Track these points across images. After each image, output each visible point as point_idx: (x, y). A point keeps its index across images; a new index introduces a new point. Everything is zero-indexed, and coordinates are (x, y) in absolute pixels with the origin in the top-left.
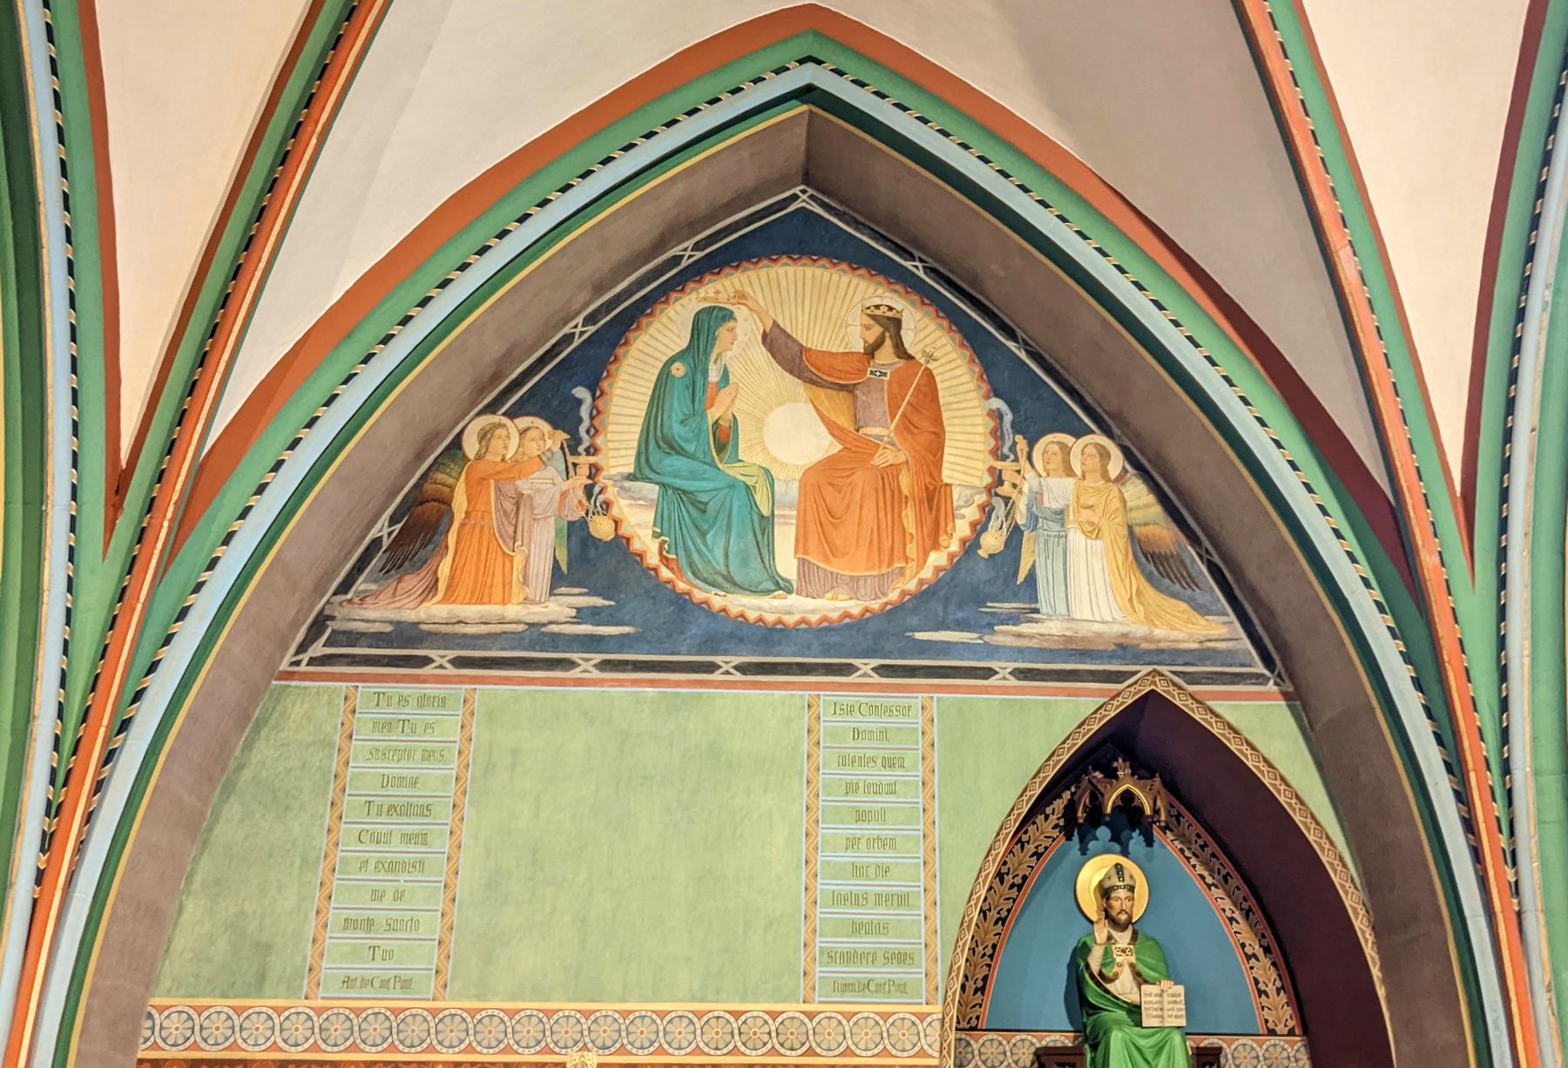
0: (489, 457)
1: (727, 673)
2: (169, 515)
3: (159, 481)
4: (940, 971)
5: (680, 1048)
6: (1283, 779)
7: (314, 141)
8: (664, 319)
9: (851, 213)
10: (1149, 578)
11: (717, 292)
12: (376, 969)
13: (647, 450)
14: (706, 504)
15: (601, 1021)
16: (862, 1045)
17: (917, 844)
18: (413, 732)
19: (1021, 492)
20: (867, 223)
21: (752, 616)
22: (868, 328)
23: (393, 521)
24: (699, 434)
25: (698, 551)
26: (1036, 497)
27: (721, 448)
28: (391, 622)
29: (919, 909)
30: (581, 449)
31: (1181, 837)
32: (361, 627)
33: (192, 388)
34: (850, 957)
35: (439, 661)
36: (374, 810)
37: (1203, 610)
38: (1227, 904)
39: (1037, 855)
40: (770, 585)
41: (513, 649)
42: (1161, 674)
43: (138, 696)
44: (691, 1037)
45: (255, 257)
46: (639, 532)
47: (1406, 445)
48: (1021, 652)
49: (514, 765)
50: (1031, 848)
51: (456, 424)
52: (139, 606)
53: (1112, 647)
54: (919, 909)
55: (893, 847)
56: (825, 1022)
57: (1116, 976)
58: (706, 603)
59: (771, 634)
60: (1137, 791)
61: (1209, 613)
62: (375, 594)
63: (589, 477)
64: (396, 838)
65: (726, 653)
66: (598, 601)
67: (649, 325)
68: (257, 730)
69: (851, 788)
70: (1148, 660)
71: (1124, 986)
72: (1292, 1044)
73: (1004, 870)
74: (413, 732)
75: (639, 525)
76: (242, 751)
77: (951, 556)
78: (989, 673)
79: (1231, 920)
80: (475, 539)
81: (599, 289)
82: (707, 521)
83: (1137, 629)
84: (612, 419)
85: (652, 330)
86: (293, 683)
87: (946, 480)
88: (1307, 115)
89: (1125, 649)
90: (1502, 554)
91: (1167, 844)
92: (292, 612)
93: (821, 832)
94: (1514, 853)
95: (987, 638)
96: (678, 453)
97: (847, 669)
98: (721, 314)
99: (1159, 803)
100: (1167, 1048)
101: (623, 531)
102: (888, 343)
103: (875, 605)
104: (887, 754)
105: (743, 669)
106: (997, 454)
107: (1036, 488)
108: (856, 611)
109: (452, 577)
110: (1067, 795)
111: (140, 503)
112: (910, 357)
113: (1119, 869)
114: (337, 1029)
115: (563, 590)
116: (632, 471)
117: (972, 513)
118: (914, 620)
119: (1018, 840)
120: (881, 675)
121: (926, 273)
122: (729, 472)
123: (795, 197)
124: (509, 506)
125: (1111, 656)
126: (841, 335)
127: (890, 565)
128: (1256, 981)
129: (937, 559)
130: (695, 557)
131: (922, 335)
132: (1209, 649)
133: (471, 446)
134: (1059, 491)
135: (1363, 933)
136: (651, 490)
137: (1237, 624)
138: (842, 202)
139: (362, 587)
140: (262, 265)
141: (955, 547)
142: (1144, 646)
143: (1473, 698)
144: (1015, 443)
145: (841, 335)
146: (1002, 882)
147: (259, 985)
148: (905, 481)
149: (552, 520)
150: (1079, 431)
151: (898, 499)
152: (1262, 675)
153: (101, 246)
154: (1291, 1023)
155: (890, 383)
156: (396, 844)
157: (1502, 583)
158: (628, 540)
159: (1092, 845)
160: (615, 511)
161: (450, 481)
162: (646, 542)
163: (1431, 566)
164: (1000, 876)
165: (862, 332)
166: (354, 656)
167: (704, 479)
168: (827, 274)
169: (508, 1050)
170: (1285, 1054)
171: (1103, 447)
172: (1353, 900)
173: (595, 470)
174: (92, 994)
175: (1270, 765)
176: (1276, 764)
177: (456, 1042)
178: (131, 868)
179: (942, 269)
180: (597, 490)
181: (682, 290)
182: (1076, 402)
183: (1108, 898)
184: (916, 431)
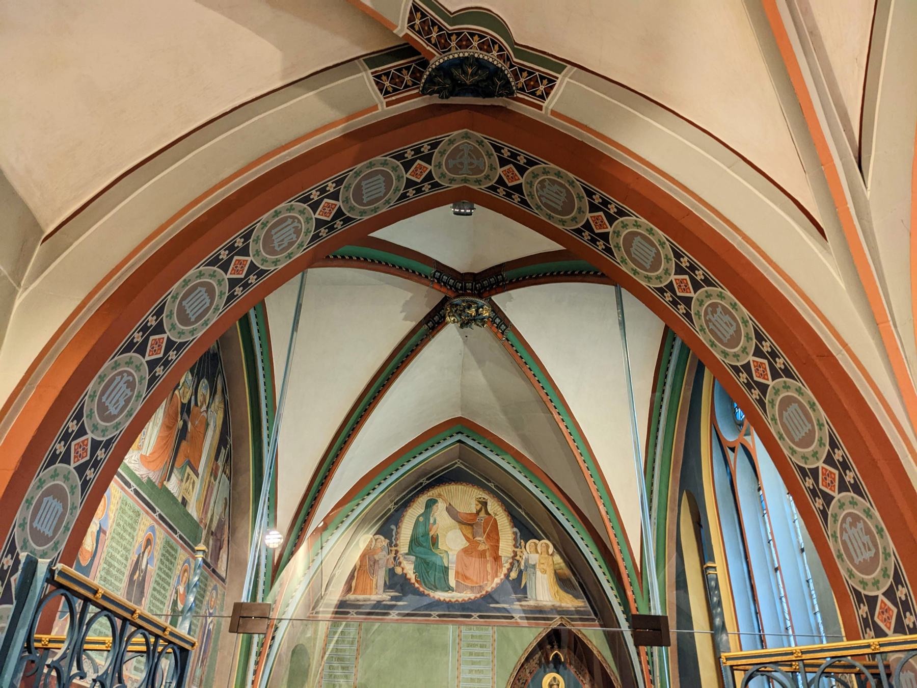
27: (433, 545)
105: (439, 616)
113: (554, 678)
123: (456, 463)
129: (497, 580)
150: (540, 539)
162: (411, 576)
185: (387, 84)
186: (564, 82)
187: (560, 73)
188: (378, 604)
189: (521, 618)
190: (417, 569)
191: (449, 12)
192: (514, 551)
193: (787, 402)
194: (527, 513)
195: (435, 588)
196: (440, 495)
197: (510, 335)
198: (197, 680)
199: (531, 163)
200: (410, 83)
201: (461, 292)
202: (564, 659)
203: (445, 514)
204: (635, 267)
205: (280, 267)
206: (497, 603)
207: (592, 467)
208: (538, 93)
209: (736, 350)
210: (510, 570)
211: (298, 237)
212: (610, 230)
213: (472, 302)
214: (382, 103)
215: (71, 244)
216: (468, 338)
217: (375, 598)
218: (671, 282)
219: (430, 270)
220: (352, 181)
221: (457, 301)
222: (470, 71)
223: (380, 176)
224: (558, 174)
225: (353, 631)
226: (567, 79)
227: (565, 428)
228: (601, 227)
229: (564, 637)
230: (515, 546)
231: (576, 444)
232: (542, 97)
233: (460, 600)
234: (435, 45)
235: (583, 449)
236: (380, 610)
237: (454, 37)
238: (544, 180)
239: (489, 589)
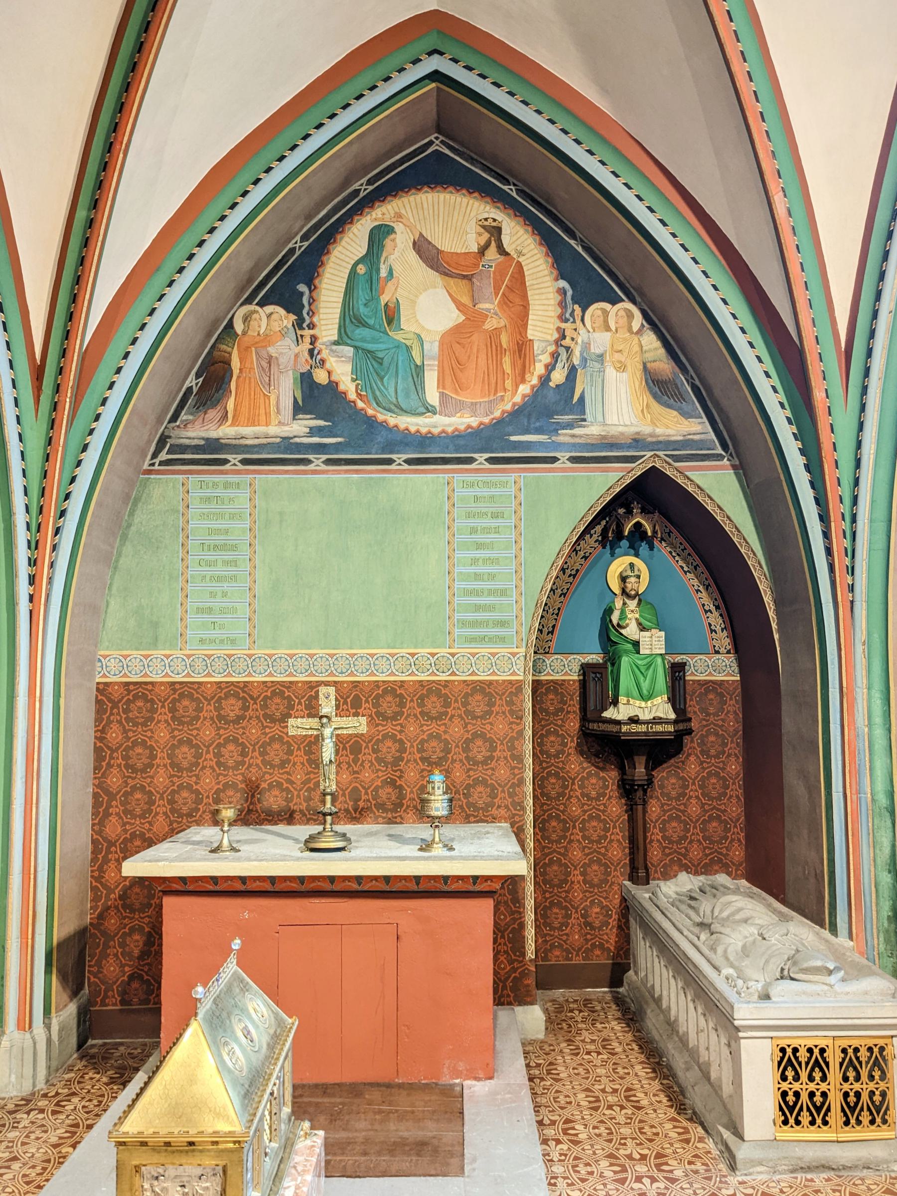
0: (250, 333)
1: (400, 464)
2: (69, 395)
3: (60, 374)
4: (524, 630)
5: (383, 673)
6: (728, 517)
7: (121, 155)
8: (351, 235)
9: (468, 152)
10: (655, 397)
11: (383, 214)
12: (216, 634)
13: (345, 324)
14: (382, 359)
15: (340, 659)
16: (481, 670)
17: (512, 562)
18: (223, 503)
19: (576, 343)
20: (479, 159)
21: (413, 429)
22: (480, 234)
23: (198, 376)
24: (376, 313)
25: (379, 389)
26: (586, 346)
27: (390, 322)
28: (203, 439)
29: (512, 597)
30: (305, 325)
31: (671, 544)
32: (187, 442)
33: (70, 317)
34: (475, 624)
35: (233, 461)
36: (206, 548)
37: (686, 415)
38: (696, 582)
39: (585, 558)
40: (423, 410)
41: (275, 453)
42: (658, 456)
43: (67, 497)
44: (388, 667)
45: (96, 232)
46: (343, 378)
47: (810, 322)
48: (575, 447)
49: (281, 521)
50: (581, 554)
51: (229, 312)
52: (60, 448)
53: (630, 441)
54: (512, 597)
55: (498, 563)
56: (461, 658)
57: (627, 625)
58: (385, 422)
59: (424, 440)
60: (643, 522)
61: (691, 417)
62: (193, 422)
63: (311, 344)
64: (220, 563)
65: (398, 452)
66: (321, 423)
67: (341, 239)
68: (135, 504)
69: (474, 531)
70: (651, 448)
71: (631, 631)
72: (728, 659)
73: (566, 566)
74: (223, 503)
75: (343, 374)
76: (129, 516)
77: (533, 387)
78: (554, 460)
79: (698, 591)
80: (247, 386)
81: (309, 218)
82: (383, 370)
83: (646, 429)
84: (322, 305)
85: (343, 243)
86: (152, 477)
87: (530, 337)
88: (758, 101)
89: (638, 442)
90: (864, 390)
91: (662, 549)
92: (146, 437)
93: (456, 556)
94: (853, 568)
95: (554, 438)
96: (364, 326)
97: (470, 460)
98: (386, 230)
99: (657, 527)
100: (653, 665)
101: (333, 378)
102: (493, 244)
103: (486, 420)
104: (494, 510)
105: (409, 462)
106: (562, 318)
107: (586, 340)
108: (475, 424)
109: (235, 410)
110: (604, 523)
111: (51, 388)
112: (507, 254)
113: (632, 565)
114: (199, 665)
115: (301, 416)
116: (336, 338)
117: (546, 359)
118: (510, 429)
119: (574, 550)
120: (490, 464)
121: (517, 194)
122: (395, 337)
123: (431, 143)
124: (265, 364)
125: (629, 447)
126: (463, 241)
127: (495, 394)
128: (710, 625)
129: (524, 389)
130: (378, 393)
131: (515, 238)
132: (689, 440)
133: (239, 327)
134: (601, 341)
135: (769, 604)
136: (349, 351)
137: (707, 424)
138: (461, 144)
139: (185, 418)
140: (101, 238)
141: (535, 381)
142: (650, 439)
143: (838, 479)
144: (573, 311)
145: (463, 241)
146: (564, 574)
147: (155, 643)
148: (504, 339)
149: (291, 372)
150: (615, 300)
151: (500, 351)
152: (721, 455)
153: (8, 247)
154: (728, 647)
155: (494, 273)
156: (220, 566)
157: (863, 408)
158: (337, 384)
159: (617, 551)
160: (328, 365)
161: (229, 349)
162: (348, 385)
163: (819, 399)
164: (563, 570)
165: (476, 238)
166: (184, 459)
167: (380, 343)
168: (453, 197)
169: (291, 675)
170: (724, 664)
171: (630, 311)
172: (764, 586)
173: (314, 339)
174: (68, 655)
175: (721, 509)
176: (724, 509)
177: (262, 671)
178: (78, 588)
179: (528, 191)
180: (316, 352)
181: (361, 214)
182: (613, 281)
183: (625, 582)
184: (511, 305)
192: (558, 329)
194: (587, 249)
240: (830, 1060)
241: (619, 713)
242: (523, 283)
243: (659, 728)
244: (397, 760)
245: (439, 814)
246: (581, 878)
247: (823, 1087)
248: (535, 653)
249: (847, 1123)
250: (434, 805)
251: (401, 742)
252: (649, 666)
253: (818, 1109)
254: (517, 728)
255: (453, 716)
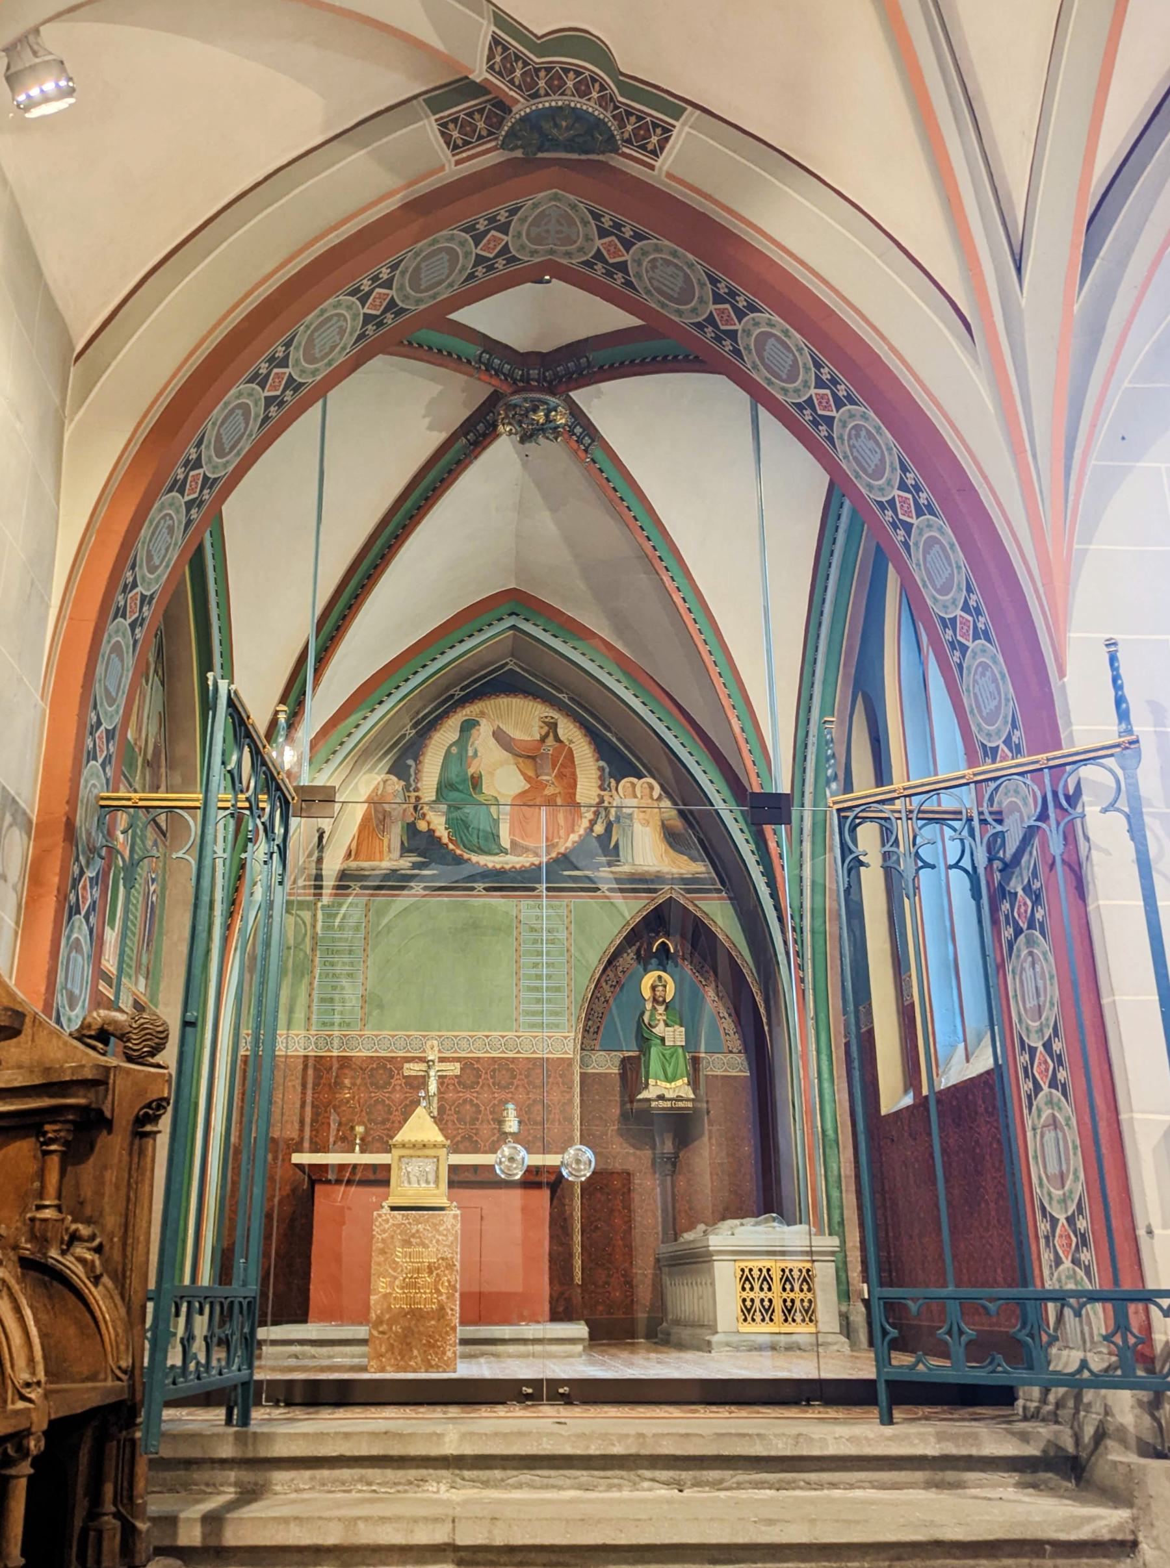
27: (474, 788)
89: (659, 878)
105: (485, 889)
113: (660, 977)
123: (507, 664)
129: (574, 837)
141: (582, 832)
150: (640, 776)
159: (650, 967)
162: (442, 832)
169: (392, 1051)
185: (455, 134)
186: (683, 131)
187: (677, 119)
188: (393, 874)
189: (611, 890)
190: (449, 824)
191: (535, 35)
192: (599, 795)
193: (932, 541)
194: (619, 739)
195: (482, 851)
196: (482, 714)
197: (598, 454)
198: (144, 969)
199: (639, 237)
200: (484, 133)
201: (523, 385)
202: (675, 949)
203: (492, 742)
204: (769, 376)
205: (319, 378)
206: (577, 869)
207: (721, 660)
208: (650, 147)
209: (880, 482)
210: (593, 823)
211: (341, 339)
212: (738, 327)
213: (540, 400)
214: (449, 161)
215: (109, 365)
216: (530, 458)
217: (386, 864)
218: (811, 397)
219: (473, 350)
220: (409, 264)
221: (516, 399)
222: (564, 124)
223: (443, 254)
224: (674, 254)
225: (357, 915)
226: (687, 129)
227: (682, 601)
228: (727, 322)
229: (674, 920)
230: (602, 788)
231: (698, 626)
232: (655, 153)
233: (518, 866)
234: (519, 87)
235: (709, 635)
236: (395, 882)
237: (542, 74)
238: (655, 260)
239: (562, 850)
240: (774, 1277)
241: (650, 1093)
242: (573, 762)
243: (681, 1104)
244: (474, 1120)
245: (512, 1130)
246: (620, 1243)
247: (770, 1295)
248: (582, 1049)
249: (786, 1320)
250: (507, 1124)
251: (477, 1106)
252: (672, 1055)
253: (767, 1311)
254: (568, 1096)
255: (517, 1086)
